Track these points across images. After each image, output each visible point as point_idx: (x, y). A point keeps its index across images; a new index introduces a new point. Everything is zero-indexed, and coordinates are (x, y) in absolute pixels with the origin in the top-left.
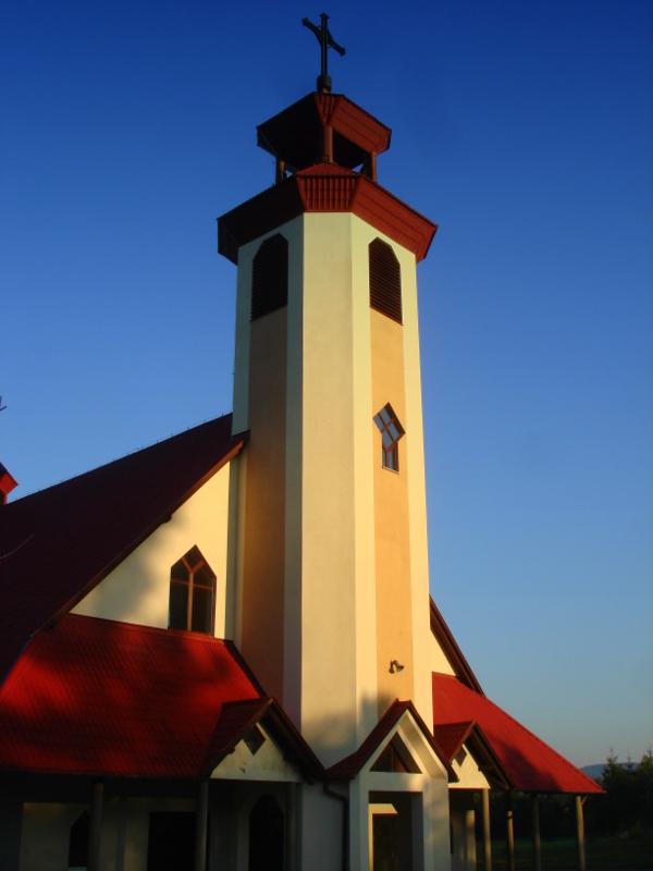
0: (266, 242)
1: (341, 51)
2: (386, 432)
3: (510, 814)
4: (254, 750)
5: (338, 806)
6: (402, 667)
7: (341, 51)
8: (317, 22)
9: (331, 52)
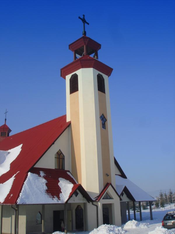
0: (72, 76)
1: (88, 24)
2: (103, 121)
3: (10, 198)
4: (76, 196)
5: (96, 207)
6: (108, 175)
7: (88, 24)
8: (82, 17)
9: (86, 24)
